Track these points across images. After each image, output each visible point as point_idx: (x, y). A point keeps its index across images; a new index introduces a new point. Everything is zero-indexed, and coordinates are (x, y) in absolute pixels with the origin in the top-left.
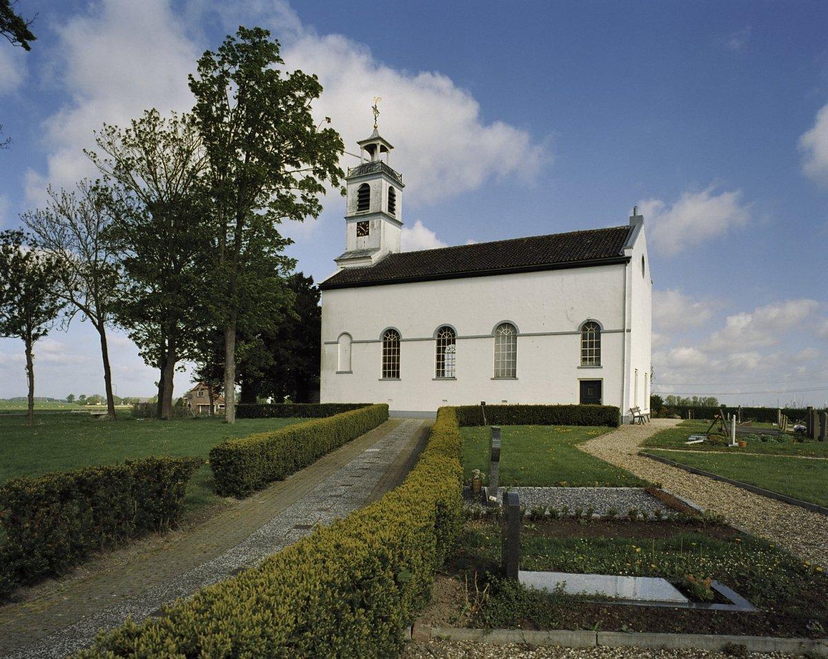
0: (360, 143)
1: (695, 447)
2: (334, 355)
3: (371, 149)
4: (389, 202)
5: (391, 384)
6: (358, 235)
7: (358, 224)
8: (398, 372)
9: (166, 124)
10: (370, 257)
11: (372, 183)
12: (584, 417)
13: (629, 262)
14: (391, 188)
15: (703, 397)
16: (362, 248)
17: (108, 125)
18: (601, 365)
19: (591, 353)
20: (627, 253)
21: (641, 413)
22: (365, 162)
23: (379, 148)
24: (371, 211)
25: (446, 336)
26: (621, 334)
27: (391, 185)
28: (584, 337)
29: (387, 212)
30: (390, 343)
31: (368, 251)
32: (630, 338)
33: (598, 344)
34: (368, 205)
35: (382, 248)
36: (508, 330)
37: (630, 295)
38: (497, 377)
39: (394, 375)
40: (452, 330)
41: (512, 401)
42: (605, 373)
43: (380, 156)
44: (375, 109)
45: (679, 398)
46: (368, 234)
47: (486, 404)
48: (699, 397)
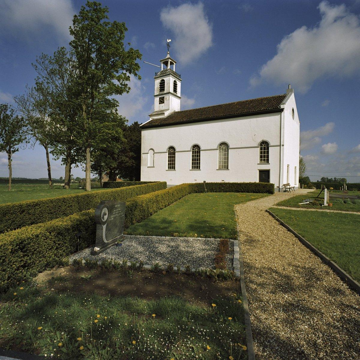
2: (147, 159)
4: (174, 88)
5: (172, 172)
6: (160, 104)
7: (160, 98)
8: (200, 166)
10: (164, 114)
11: (166, 79)
12: (256, 188)
13: (283, 111)
14: (175, 81)
15: (339, 178)
16: (161, 110)
17: (44, 54)
18: (269, 163)
19: (265, 157)
20: (282, 106)
21: (290, 186)
23: (169, 63)
24: (165, 92)
25: (196, 150)
26: (279, 147)
27: (174, 80)
28: (261, 149)
29: (173, 92)
30: (171, 153)
31: (164, 111)
32: (283, 149)
33: (268, 152)
34: (164, 89)
35: (170, 109)
36: (224, 146)
37: (284, 128)
38: (220, 169)
39: (173, 168)
41: (227, 181)
42: (272, 167)
45: (327, 178)
46: (164, 103)
47: (206, 182)
48: (337, 178)
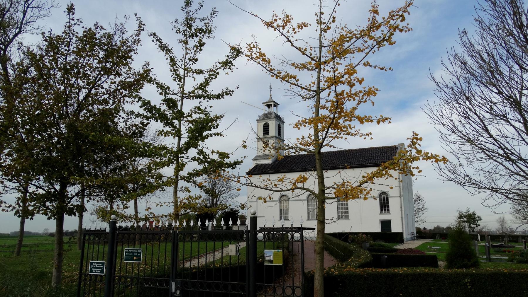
0: (263, 103)
1: (435, 250)
3: (269, 106)
9: (99, 31)
22: (266, 112)
34: (269, 133)
40: (384, 193)
43: (273, 109)
44: (270, 88)
